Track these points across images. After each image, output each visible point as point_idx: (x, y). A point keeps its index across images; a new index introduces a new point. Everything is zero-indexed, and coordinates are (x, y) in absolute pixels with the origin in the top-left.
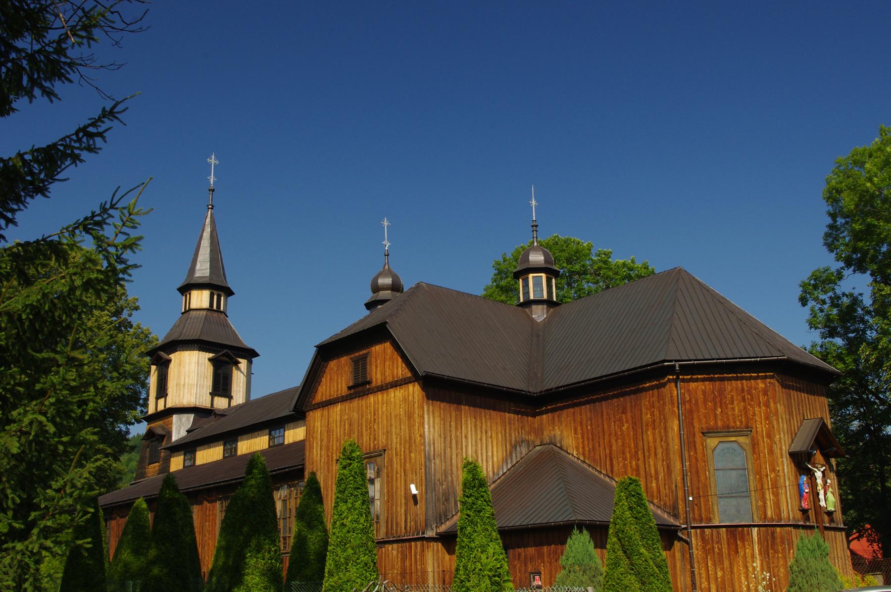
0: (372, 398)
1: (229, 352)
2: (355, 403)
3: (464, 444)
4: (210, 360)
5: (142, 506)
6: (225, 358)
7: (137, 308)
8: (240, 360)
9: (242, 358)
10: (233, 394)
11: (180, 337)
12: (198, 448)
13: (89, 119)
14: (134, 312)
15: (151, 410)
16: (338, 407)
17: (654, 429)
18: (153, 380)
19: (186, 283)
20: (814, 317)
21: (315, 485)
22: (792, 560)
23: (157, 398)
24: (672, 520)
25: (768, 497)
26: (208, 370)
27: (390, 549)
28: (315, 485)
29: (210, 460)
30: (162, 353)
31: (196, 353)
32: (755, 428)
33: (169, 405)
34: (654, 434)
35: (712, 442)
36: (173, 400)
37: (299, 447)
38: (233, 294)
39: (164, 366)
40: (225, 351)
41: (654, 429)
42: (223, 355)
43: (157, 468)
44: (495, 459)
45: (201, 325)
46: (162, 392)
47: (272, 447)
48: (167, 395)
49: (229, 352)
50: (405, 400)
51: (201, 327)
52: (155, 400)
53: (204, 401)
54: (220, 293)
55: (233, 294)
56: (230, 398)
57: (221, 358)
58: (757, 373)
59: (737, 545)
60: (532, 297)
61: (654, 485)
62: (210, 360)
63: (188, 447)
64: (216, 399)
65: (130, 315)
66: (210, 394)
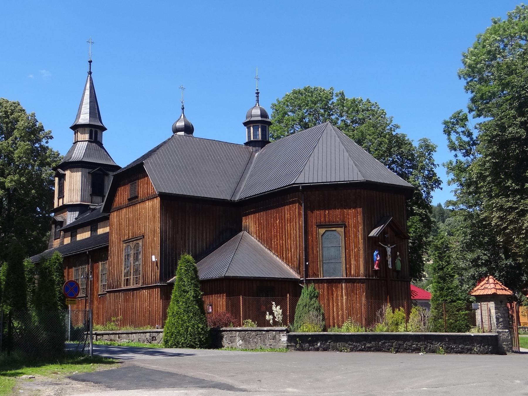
0: (138, 206)
2: (131, 209)
3: (187, 232)
7: (51, 138)
12: (78, 231)
14: (50, 140)
15: (56, 206)
16: (124, 210)
17: (290, 223)
18: (56, 189)
19: (75, 124)
21: (182, 253)
23: (59, 199)
24: (297, 276)
25: (352, 263)
27: (145, 291)
28: (182, 253)
29: (84, 238)
30: (59, 169)
32: (347, 222)
33: (65, 202)
34: (290, 225)
35: (322, 231)
36: (67, 200)
37: (106, 235)
38: (106, 129)
39: (62, 177)
41: (290, 223)
43: (59, 242)
44: (208, 240)
45: (84, 151)
46: (61, 195)
48: (64, 197)
50: (153, 206)
51: (84, 153)
52: (57, 199)
54: (96, 129)
55: (106, 129)
57: (97, 172)
59: (333, 290)
60: (252, 139)
61: (290, 255)
62: (89, 173)
63: (73, 230)
65: (47, 142)
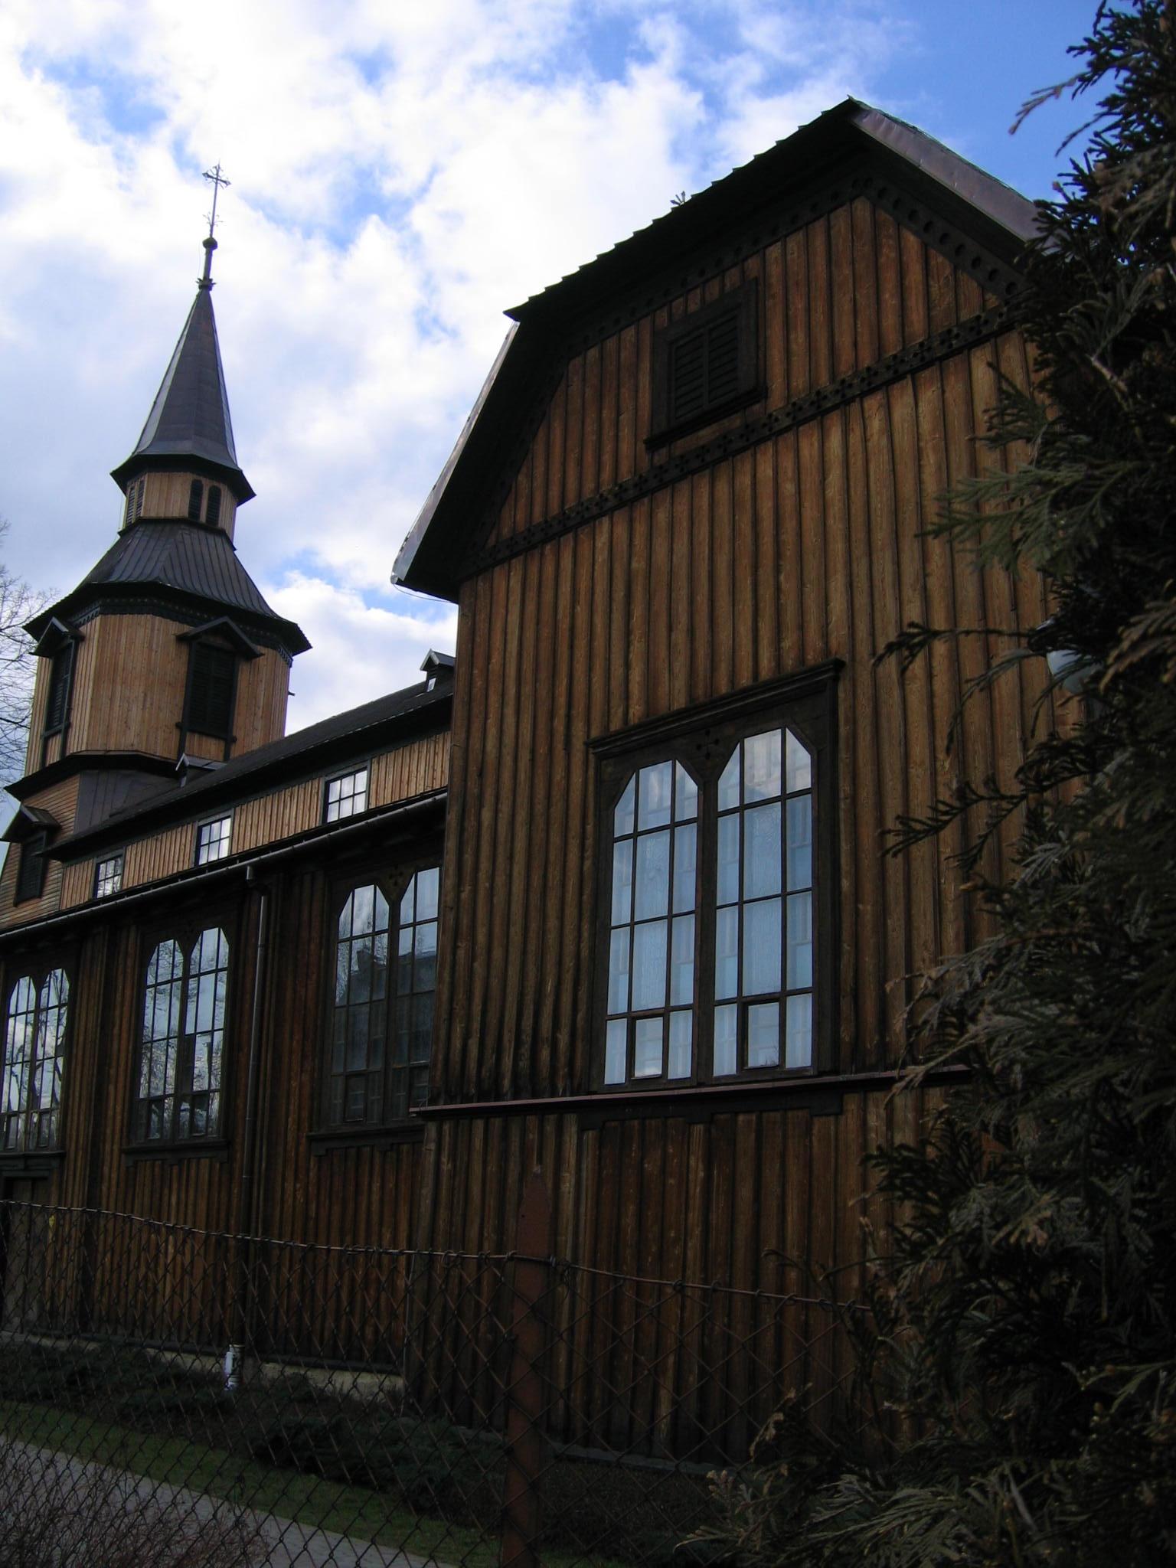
1: (233, 625)
4: (181, 639)
5: (1101, 824)
6: (218, 641)
8: (260, 649)
9: (266, 646)
10: (238, 732)
11: (110, 574)
13: (1060, 175)
20: (334, 1507)
22: (908, 1377)
26: (174, 665)
31: (145, 619)
40: (225, 619)
42: (215, 631)
47: (120, 856)
48: (69, 726)
49: (233, 625)
53: (161, 747)
56: (229, 740)
58: (294, 849)
64: (194, 741)
66: (178, 725)
